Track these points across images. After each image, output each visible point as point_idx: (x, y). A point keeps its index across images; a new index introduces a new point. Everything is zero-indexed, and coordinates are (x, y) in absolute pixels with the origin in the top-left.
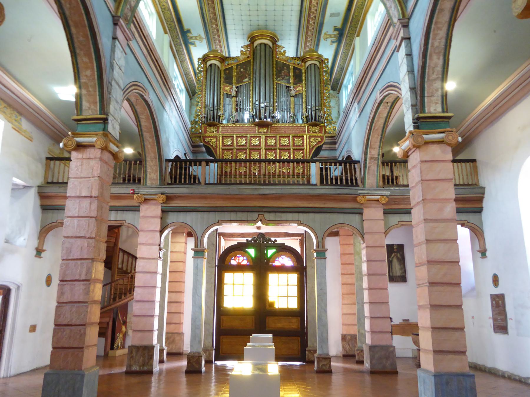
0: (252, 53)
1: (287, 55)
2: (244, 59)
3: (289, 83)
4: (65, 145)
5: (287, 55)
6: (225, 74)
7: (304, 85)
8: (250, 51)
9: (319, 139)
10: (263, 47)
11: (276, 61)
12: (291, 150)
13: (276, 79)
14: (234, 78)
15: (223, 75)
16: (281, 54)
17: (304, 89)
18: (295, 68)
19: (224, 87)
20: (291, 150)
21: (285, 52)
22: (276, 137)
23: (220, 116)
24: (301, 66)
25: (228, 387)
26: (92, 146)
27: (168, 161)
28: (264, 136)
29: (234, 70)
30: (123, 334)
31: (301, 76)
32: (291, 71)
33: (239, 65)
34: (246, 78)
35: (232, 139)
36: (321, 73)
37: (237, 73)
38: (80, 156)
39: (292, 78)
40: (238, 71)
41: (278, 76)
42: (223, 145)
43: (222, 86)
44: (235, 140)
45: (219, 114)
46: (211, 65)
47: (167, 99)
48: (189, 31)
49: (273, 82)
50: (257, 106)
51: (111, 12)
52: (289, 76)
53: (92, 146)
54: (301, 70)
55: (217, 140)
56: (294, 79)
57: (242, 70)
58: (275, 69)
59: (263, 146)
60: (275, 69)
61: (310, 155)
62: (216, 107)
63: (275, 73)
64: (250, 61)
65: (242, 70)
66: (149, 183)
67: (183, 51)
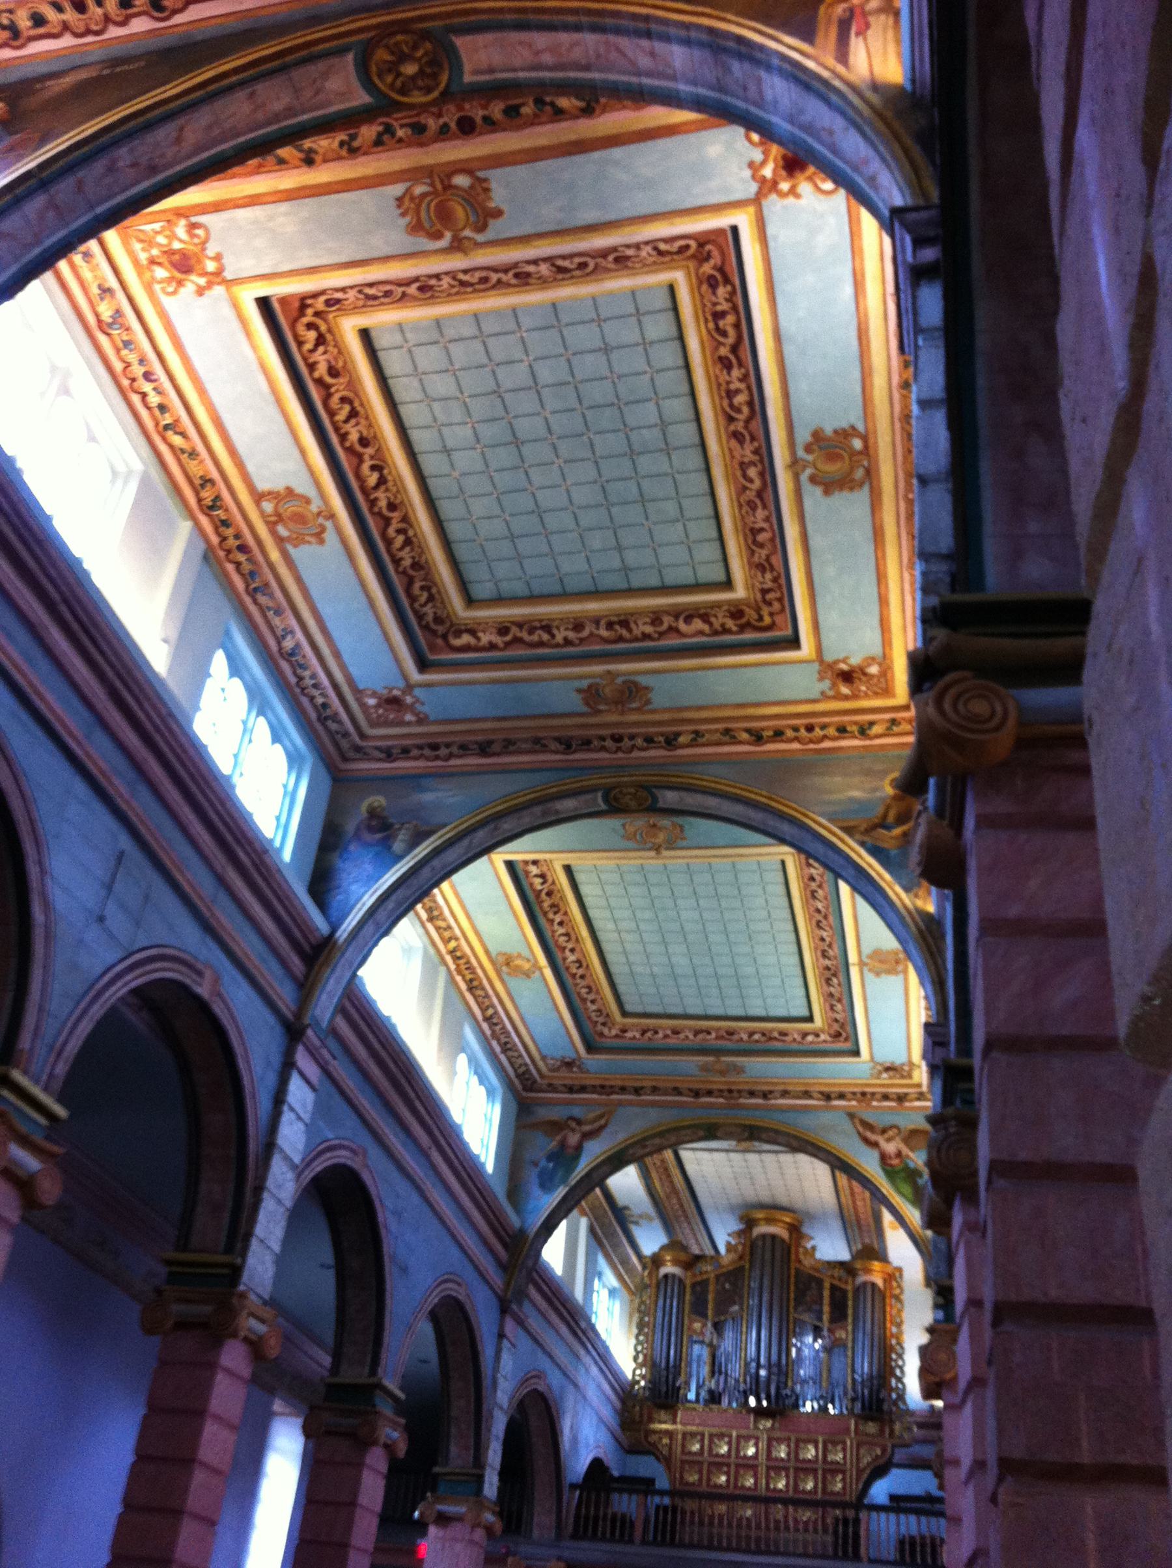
0: (748, 1250)
1: (818, 1255)
2: (733, 1262)
3: (820, 1319)
4: (421, 1514)
5: (818, 1255)
6: (693, 1292)
7: (850, 1328)
8: (744, 1245)
9: (879, 1452)
10: (768, 1242)
11: (797, 1270)
12: (820, 1472)
13: (795, 1309)
14: (710, 1306)
15: (688, 1297)
16: (806, 1251)
17: (850, 1337)
18: (833, 1288)
19: (691, 1322)
20: (820, 1472)
21: (814, 1248)
22: (789, 1439)
23: (679, 1388)
24: (846, 1283)
25: (253, 1322)
26: (459, 1519)
27: (573, 1486)
28: (765, 1436)
29: (711, 1288)
30: (836, 1225)
31: (845, 1306)
32: (826, 1293)
33: (723, 1274)
34: (735, 1303)
35: (702, 1441)
36: (888, 1301)
37: (718, 1293)
38: (441, 1533)
39: (826, 1309)
40: (719, 1287)
41: (799, 1302)
42: (683, 1452)
43: (686, 1322)
44: (706, 1442)
45: (678, 1384)
46: (666, 1276)
47: (577, 1357)
48: (626, 1208)
49: (788, 1315)
50: (753, 1371)
51: (491, 1288)
52: (821, 1304)
53: (459, 1519)
54: (844, 1293)
55: (671, 1439)
56: (832, 1313)
57: (727, 1286)
58: (792, 1288)
59: (762, 1458)
60: (792, 1288)
61: (858, 1480)
62: (672, 1370)
63: (792, 1295)
64: (742, 1268)
65: (727, 1286)
66: (536, 1533)
67: (615, 1231)
